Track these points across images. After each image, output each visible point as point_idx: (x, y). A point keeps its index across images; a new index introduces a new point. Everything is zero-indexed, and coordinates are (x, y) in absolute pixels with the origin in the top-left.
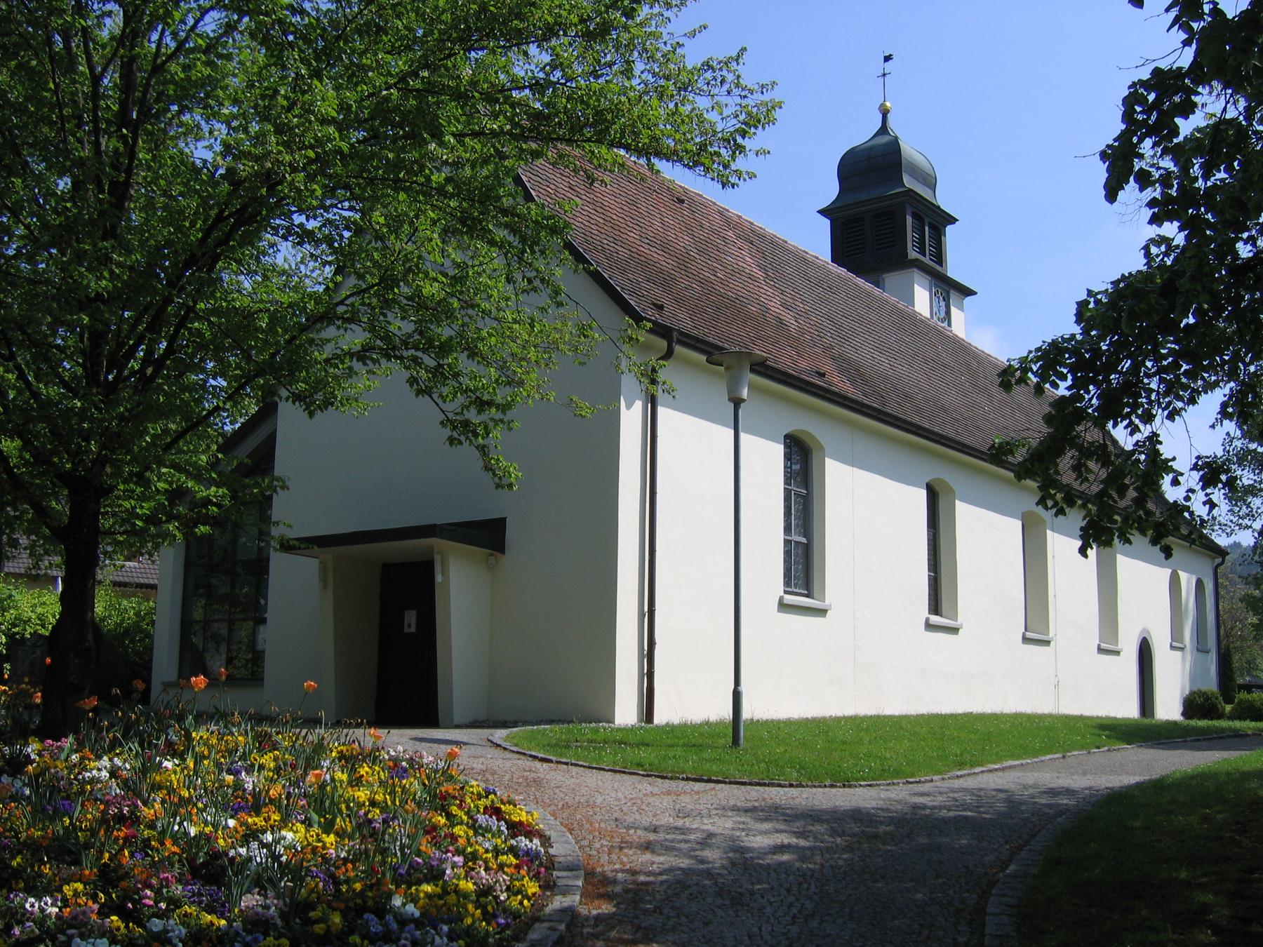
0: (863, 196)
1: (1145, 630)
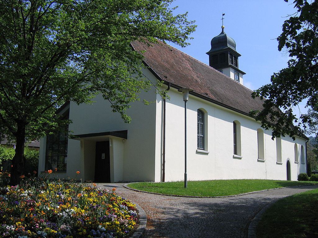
0: (217, 49)
1: (288, 158)
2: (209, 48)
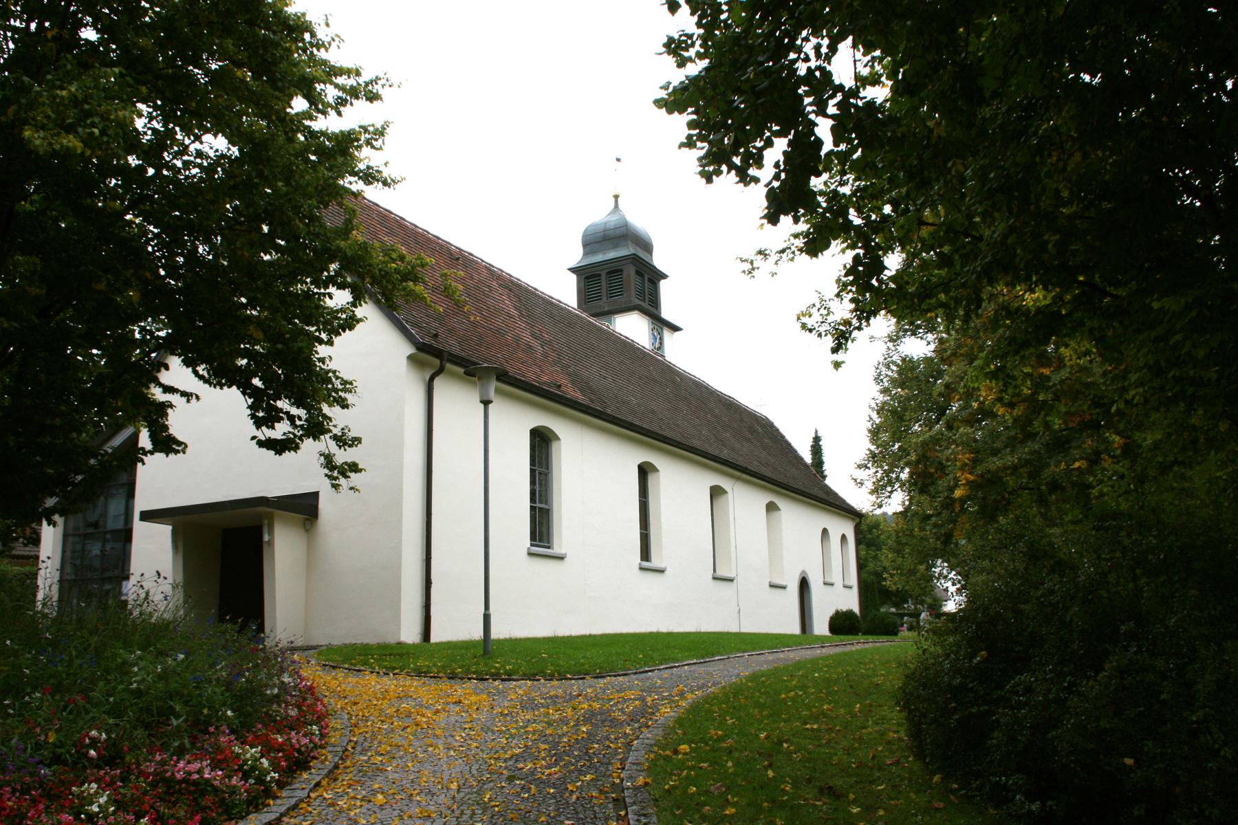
0: (599, 258)
1: (803, 572)
2: (576, 255)
